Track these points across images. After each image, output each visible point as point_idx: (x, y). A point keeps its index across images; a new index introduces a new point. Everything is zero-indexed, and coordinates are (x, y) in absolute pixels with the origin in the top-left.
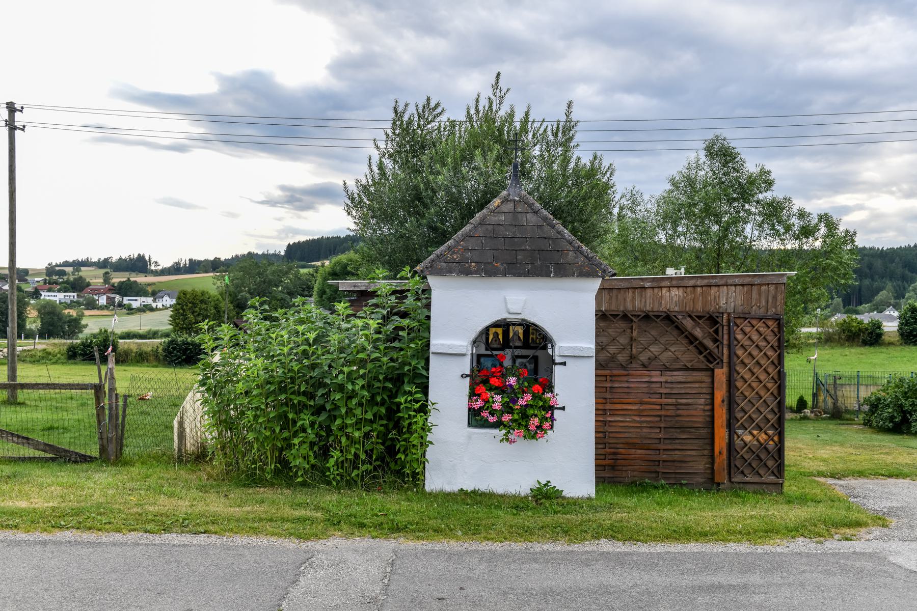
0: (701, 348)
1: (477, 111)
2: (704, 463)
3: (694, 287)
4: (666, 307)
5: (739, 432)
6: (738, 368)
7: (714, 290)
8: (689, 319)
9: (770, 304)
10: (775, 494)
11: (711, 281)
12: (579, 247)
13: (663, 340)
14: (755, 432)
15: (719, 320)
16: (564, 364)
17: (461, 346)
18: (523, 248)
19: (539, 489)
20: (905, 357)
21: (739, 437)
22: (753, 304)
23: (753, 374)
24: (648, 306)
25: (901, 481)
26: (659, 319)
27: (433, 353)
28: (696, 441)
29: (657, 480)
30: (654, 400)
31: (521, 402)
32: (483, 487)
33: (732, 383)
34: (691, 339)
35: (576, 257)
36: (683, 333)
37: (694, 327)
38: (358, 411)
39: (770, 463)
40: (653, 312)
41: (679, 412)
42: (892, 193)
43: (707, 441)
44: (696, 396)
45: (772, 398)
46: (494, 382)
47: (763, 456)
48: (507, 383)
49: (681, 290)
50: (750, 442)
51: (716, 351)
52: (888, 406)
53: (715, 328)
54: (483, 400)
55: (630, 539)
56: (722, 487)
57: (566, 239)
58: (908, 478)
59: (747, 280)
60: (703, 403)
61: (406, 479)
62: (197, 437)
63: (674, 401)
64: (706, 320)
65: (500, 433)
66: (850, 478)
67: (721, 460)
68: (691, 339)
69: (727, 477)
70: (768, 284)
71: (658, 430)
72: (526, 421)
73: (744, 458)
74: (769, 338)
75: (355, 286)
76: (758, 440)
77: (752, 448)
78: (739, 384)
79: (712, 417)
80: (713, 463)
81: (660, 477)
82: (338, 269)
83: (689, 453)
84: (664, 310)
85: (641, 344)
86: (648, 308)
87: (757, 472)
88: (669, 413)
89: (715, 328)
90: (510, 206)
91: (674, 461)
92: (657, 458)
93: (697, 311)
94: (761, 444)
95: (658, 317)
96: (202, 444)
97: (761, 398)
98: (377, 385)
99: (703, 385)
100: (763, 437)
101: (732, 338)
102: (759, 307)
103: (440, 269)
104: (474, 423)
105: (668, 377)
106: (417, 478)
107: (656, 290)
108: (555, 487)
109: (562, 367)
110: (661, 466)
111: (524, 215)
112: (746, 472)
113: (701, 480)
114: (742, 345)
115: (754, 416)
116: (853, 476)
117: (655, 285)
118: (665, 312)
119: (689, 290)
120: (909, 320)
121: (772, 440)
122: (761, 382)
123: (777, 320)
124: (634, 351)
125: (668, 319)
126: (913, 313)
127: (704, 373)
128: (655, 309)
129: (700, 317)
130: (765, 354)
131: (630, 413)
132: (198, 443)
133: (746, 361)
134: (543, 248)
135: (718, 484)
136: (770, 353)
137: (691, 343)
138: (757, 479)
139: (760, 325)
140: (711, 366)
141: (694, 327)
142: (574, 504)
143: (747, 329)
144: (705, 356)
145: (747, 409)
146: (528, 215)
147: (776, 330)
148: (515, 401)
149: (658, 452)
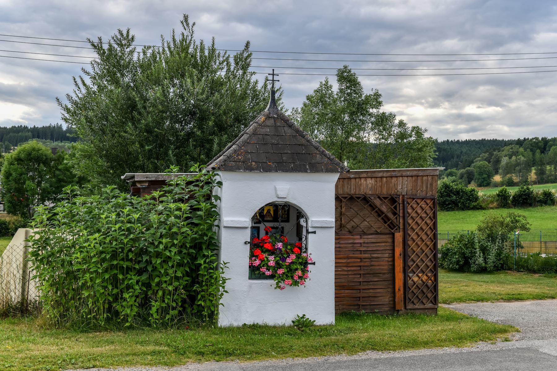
0: (386, 219)
1: (174, 40)
2: (388, 297)
3: (382, 177)
4: (364, 191)
5: (411, 275)
6: (409, 232)
7: (394, 180)
8: (378, 199)
9: (428, 189)
10: (433, 315)
11: (393, 173)
12: (323, 151)
13: (361, 214)
14: (420, 275)
15: (397, 200)
16: (314, 232)
17: (245, 221)
18: (286, 152)
19: (298, 321)
20: (442, 219)
21: (410, 278)
22: (418, 189)
23: (419, 236)
24: (352, 190)
25: (485, 303)
26: (360, 200)
27: (225, 227)
28: (383, 282)
29: (358, 310)
30: (357, 255)
31: (289, 260)
32: (260, 322)
33: (406, 241)
34: (380, 213)
35: (322, 158)
36: (374, 209)
37: (381, 205)
38: (171, 271)
39: (429, 295)
40: (355, 194)
41: (373, 263)
42: (422, 104)
43: (390, 282)
44: (384, 252)
45: (430, 252)
46: (268, 246)
47: (425, 291)
48: (276, 247)
49: (373, 179)
50: (417, 281)
51: (395, 221)
52: (455, 253)
53: (395, 205)
54: (260, 260)
55: (385, 349)
56: (400, 313)
57: (313, 146)
58: (489, 302)
59: (415, 173)
60: (387, 256)
61: (204, 319)
62: (3, 298)
63: (369, 255)
64: (389, 200)
65: (273, 282)
66: (455, 303)
67: (399, 295)
68: (380, 213)
69: (403, 306)
70: (427, 176)
71: (359, 276)
72: (291, 273)
73: (413, 292)
74: (428, 212)
75: (147, 178)
76: (422, 280)
77: (419, 286)
78: (410, 243)
79: (394, 265)
80: (394, 297)
81: (360, 308)
82: (22, 156)
83: (378, 291)
84: (363, 193)
85: (348, 217)
86: (352, 192)
87: (422, 301)
88: (366, 264)
89: (395, 205)
90: (272, 121)
91: (369, 297)
92: (359, 295)
93: (383, 194)
94: (424, 283)
95: (358, 198)
96: (7, 303)
97: (424, 252)
98: (185, 251)
99: (387, 244)
100: (425, 278)
101: (406, 212)
102: (422, 191)
103: (231, 166)
104: (253, 276)
105: (365, 240)
106: (213, 316)
107: (357, 180)
108: (308, 319)
109: (313, 235)
110: (361, 300)
111: (282, 128)
112: (415, 302)
113: (387, 309)
114: (411, 217)
115: (419, 264)
116: (457, 302)
117: (357, 176)
118: (363, 195)
119: (378, 179)
120: (443, 193)
121: (431, 280)
122: (423, 241)
123: (432, 199)
124: (343, 222)
125: (365, 199)
126: (446, 189)
127: (388, 236)
128: (357, 193)
129: (385, 198)
130: (426, 222)
131: (340, 265)
132: (4, 302)
133: (414, 227)
134: (299, 152)
135: (398, 311)
136: (428, 222)
137: (379, 216)
138: (422, 306)
139: (422, 204)
140: (393, 231)
141: (381, 205)
142: (324, 330)
143: (415, 206)
144: (388, 225)
145: (415, 259)
146: (285, 128)
147: (432, 206)
148: (284, 260)
149: (359, 291)
